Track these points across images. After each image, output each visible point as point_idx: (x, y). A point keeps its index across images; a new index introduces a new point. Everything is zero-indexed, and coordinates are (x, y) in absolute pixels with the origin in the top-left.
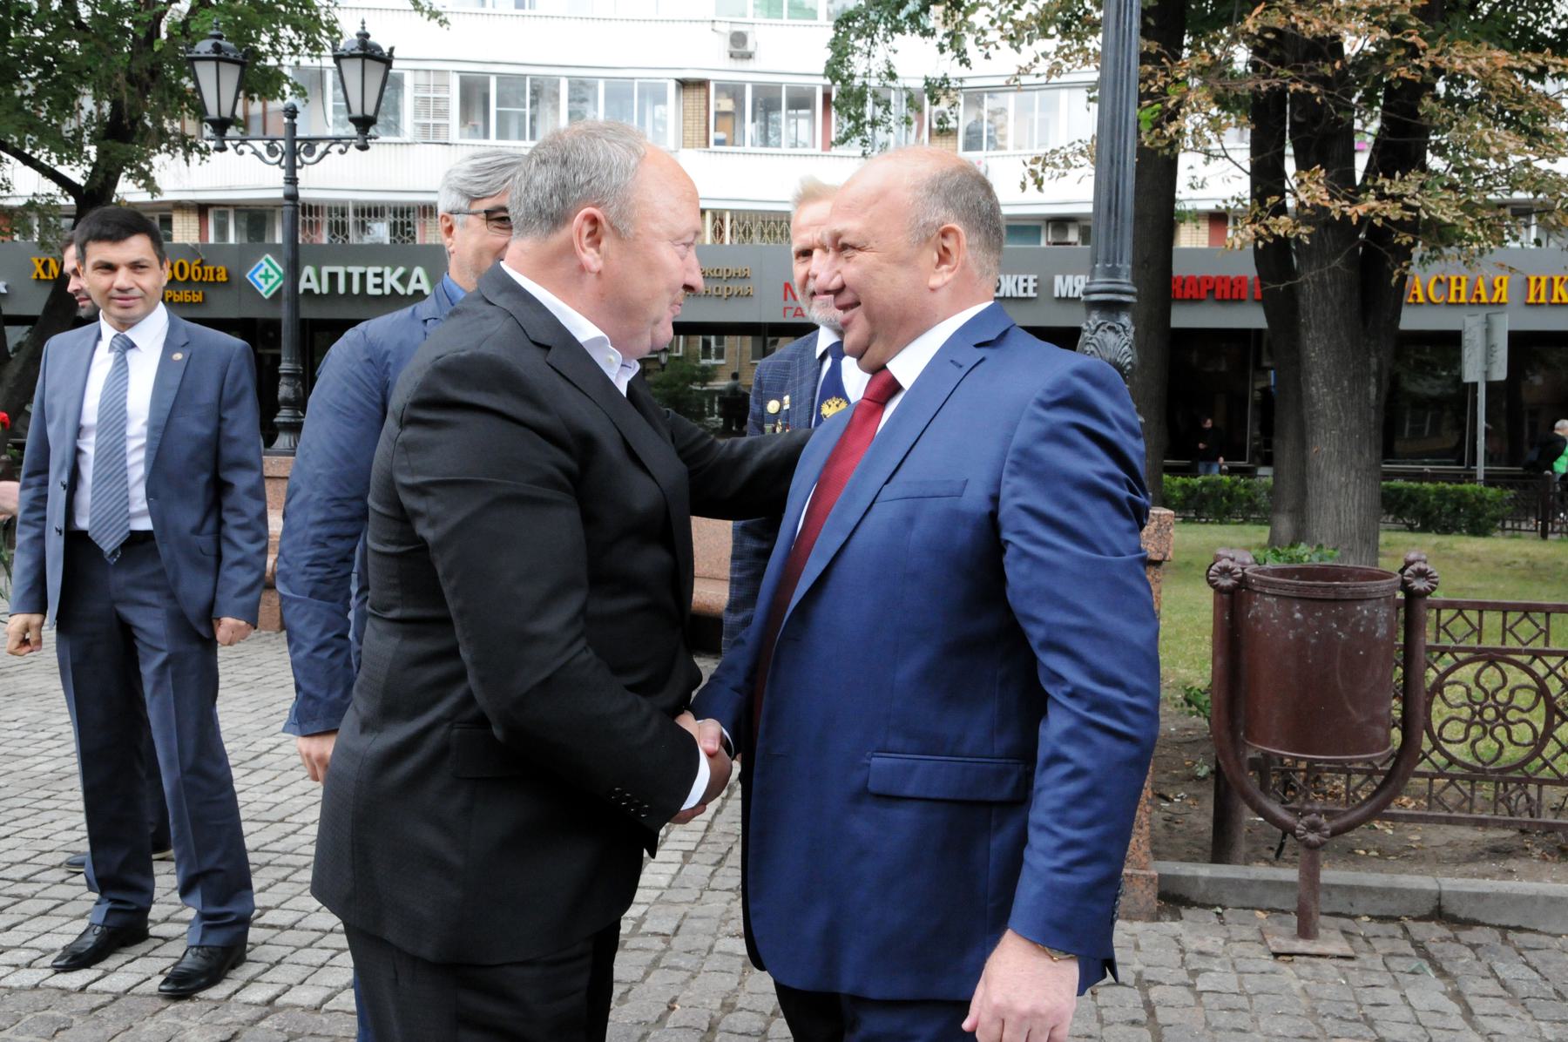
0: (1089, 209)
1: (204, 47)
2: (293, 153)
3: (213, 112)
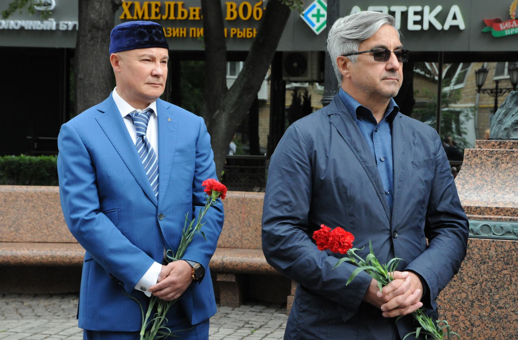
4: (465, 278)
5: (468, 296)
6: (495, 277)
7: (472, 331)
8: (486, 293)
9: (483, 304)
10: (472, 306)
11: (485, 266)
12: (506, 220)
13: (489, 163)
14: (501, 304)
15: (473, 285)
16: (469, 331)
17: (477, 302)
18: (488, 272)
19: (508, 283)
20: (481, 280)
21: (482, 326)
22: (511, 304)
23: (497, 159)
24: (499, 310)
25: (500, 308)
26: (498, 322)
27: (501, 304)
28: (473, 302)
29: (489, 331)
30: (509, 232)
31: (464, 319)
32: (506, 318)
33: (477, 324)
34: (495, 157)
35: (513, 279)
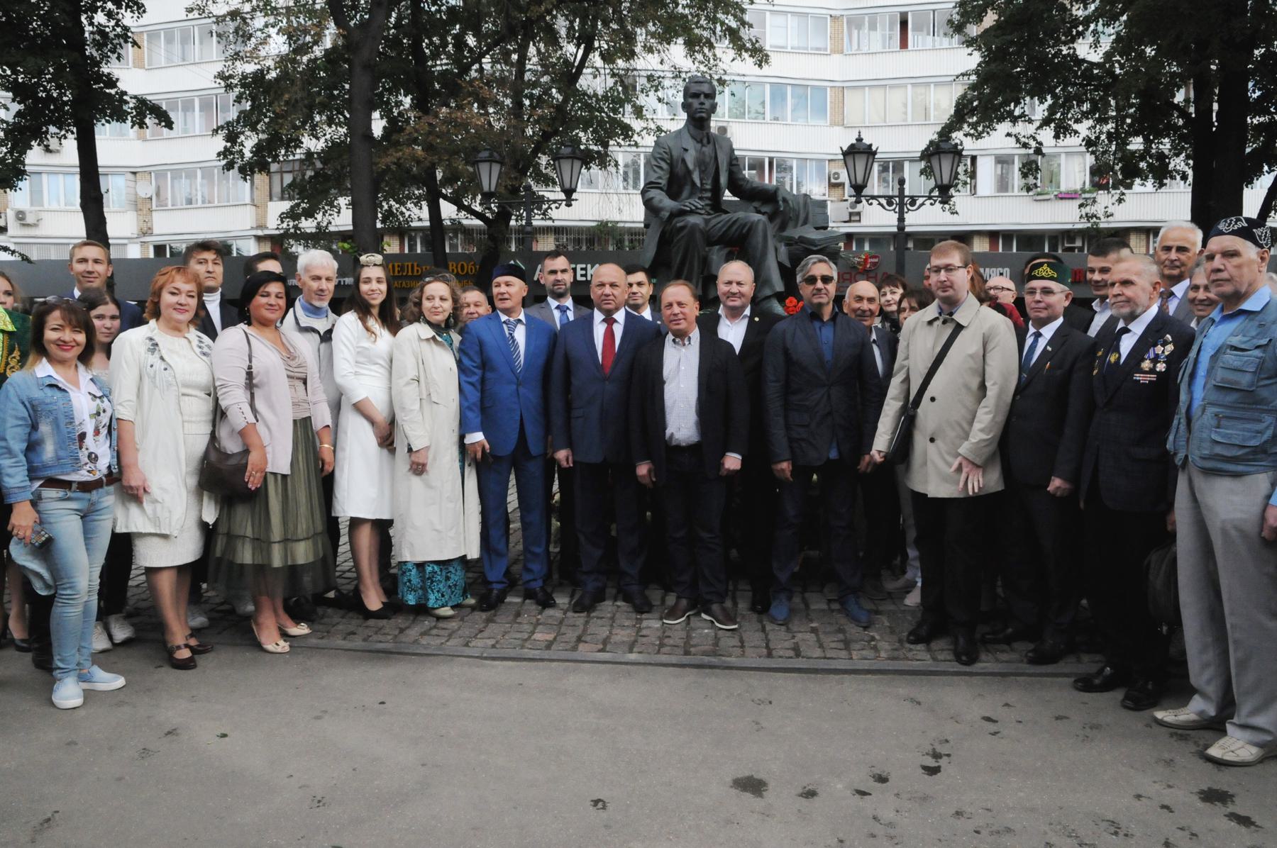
0: (351, 228)
1: (484, 154)
2: (902, 205)
3: (486, 189)
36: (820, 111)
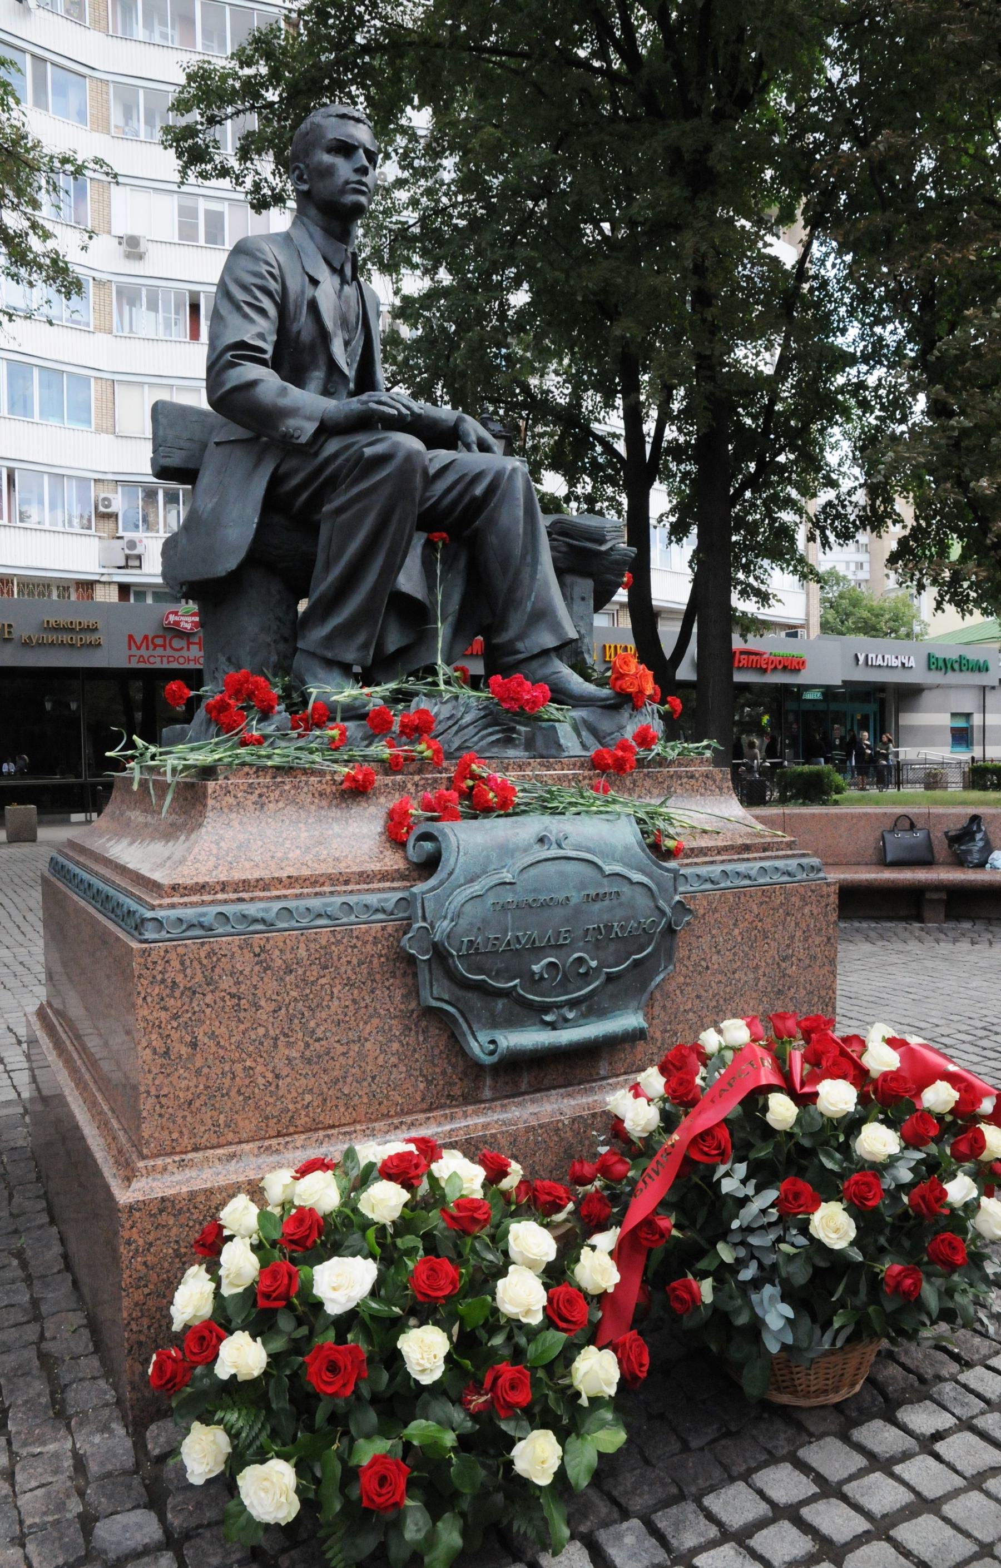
4: (262, 1003)
5: (267, 1031)
6: (308, 991)
7: (277, 1086)
8: (296, 1021)
9: (292, 1040)
10: (275, 1046)
11: (292, 976)
12: (185, 905)
13: (249, 803)
14: (319, 1033)
15: (275, 1011)
16: (272, 1088)
17: (282, 1038)
18: (297, 986)
19: (328, 998)
20: (287, 1001)
21: (293, 1074)
22: (334, 1030)
23: (260, 796)
24: (317, 1044)
25: (318, 1040)
26: (316, 1063)
27: (319, 1033)
28: (276, 1039)
29: (303, 1081)
30: (256, 921)
31: (264, 1069)
32: (328, 1054)
33: (284, 1073)
34: (257, 792)
35: (335, 991)
36: (81, 413)
